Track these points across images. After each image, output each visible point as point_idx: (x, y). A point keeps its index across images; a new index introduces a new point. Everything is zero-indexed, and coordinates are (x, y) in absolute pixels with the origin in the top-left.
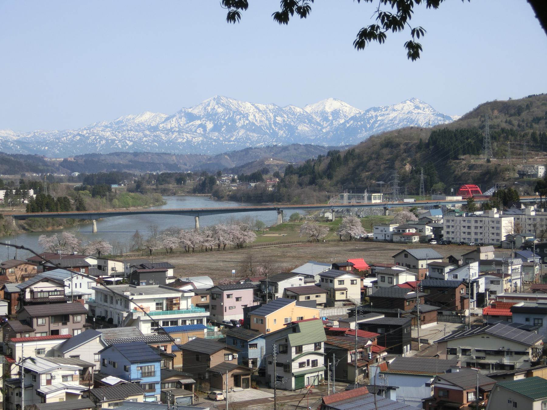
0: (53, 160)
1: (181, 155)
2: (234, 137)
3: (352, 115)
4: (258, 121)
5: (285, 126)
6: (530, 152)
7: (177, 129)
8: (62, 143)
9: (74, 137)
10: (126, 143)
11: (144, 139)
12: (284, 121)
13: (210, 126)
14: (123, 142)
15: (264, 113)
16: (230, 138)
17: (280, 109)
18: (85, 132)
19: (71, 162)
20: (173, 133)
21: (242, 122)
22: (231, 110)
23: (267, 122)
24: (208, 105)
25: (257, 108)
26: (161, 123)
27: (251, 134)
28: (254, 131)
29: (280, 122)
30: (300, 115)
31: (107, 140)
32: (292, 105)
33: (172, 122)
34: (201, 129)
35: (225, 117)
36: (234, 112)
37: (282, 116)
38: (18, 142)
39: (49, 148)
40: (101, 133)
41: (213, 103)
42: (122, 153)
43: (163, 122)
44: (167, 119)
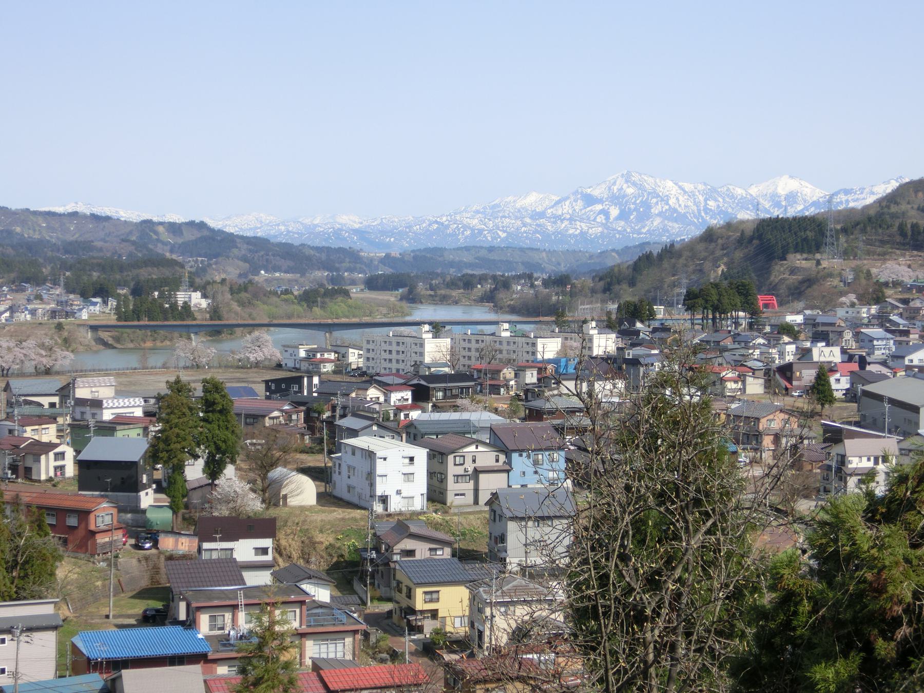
0: (372, 255)
1: (554, 251)
2: (647, 228)
3: (815, 199)
4: (683, 206)
5: (719, 214)
6: (894, 250)
7: (568, 216)
8: (414, 233)
9: (430, 225)
10: (498, 234)
11: (523, 229)
12: (718, 207)
13: (614, 212)
14: (494, 233)
15: (691, 195)
16: (640, 229)
17: (714, 190)
18: (444, 219)
19: (394, 258)
20: (562, 221)
21: (659, 207)
22: (646, 191)
23: (695, 208)
24: (614, 183)
25: (681, 188)
26: (550, 208)
27: (670, 224)
28: (676, 220)
29: (713, 208)
30: (741, 199)
31: (473, 230)
32: (730, 185)
33: (564, 207)
34: (603, 217)
35: (636, 201)
36: (649, 194)
37: (716, 200)
38: (356, 231)
39: (396, 239)
40: (466, 221)
41: (620, 182)
42: (474, 247)
43: (552, 207)
44: (558, 203)
